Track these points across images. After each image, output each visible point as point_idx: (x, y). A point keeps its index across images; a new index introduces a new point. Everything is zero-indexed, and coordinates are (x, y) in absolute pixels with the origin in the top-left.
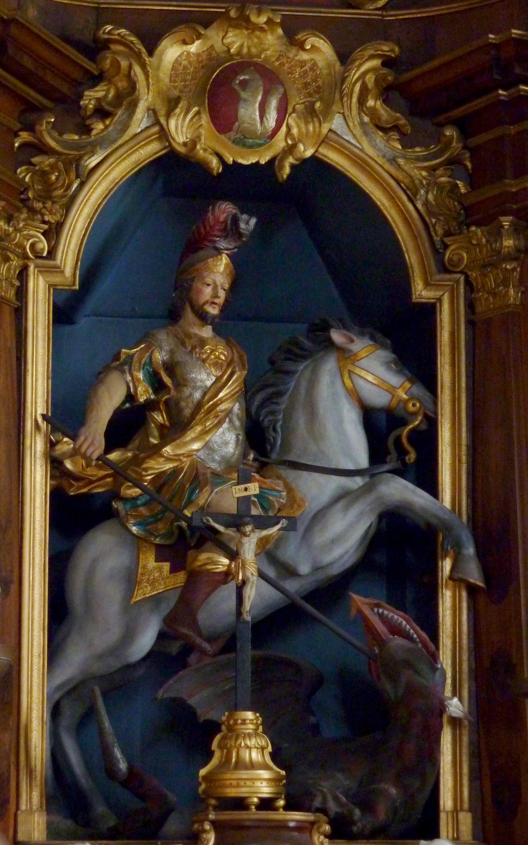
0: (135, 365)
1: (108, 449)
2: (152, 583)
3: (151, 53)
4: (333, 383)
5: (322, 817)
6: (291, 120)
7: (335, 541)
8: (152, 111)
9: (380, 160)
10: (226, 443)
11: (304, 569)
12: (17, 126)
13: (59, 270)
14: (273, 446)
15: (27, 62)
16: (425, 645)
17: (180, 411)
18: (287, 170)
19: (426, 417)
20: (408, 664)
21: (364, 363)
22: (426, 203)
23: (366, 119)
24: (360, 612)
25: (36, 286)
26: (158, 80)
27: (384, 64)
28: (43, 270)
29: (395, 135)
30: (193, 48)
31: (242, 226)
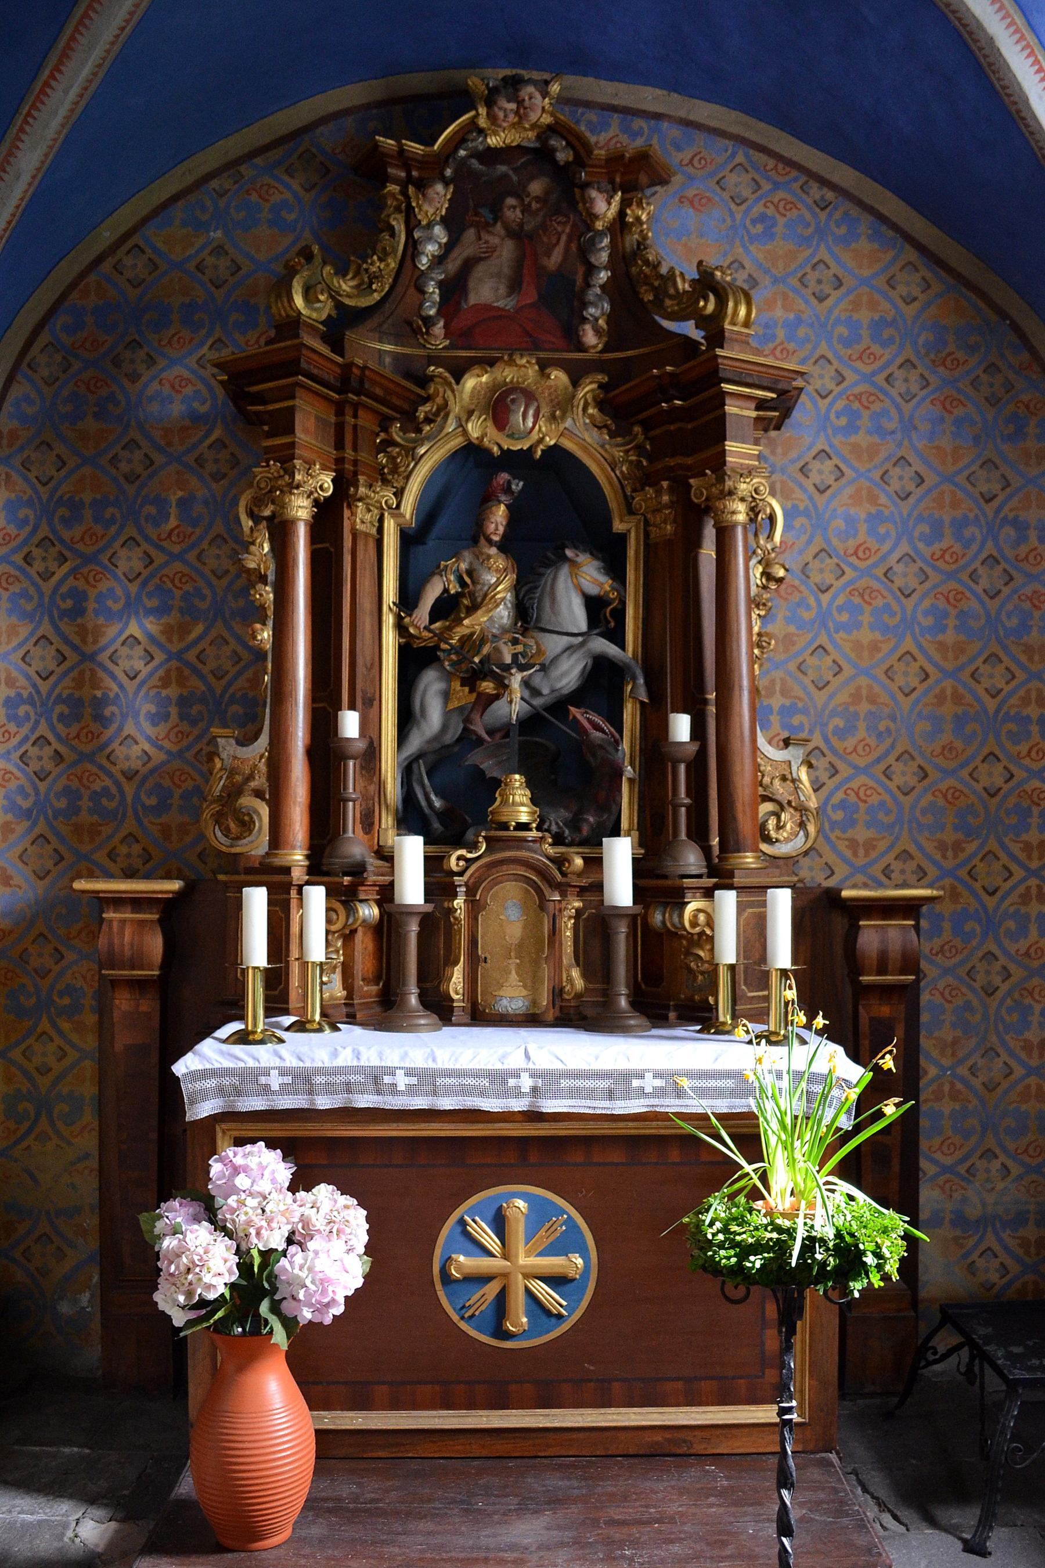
0: (449, 571)
1: (432, 622)
2: (459, 699)
3: (458, 383)
4: (566, 580)
5: (547, 834)
6: (542, 422)
7: (564, 675)
8: (459, 419)
9: (596, 446)
10: (502, 618)
11: (546, 691)
12: (378, 429)
13: (402, 516)
14: (532, 618)
15: (379, 391)
16: (613, 736)
17: (476, 599)
18: (539, 453)
19: (620, 600)
20: (601, 747)
21: (584, 569)
22: (622, 472)
23: (587, 421)
24: (575, 717)
25: (389, 524)
26: (462, 400)
27: (599, 387)
28: (393, 516)
29: (605, 431)
30: (484, 379)
31: (514, 487)
